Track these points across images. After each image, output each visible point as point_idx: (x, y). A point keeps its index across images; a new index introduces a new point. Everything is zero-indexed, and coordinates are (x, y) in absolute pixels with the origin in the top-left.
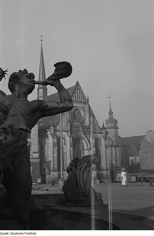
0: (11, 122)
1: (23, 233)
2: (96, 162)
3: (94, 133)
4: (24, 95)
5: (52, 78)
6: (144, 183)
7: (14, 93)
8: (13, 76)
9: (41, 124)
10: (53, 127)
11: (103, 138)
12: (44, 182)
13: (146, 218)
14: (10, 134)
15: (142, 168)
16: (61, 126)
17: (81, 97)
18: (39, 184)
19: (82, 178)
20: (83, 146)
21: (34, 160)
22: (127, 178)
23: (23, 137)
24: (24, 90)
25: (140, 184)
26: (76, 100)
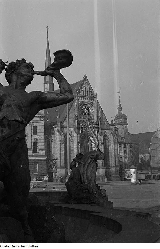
0: (6, 113)
1: (24, 246)
2: (101, 158)
3: (101, 129)
4: (21, 86)
5: (52, 67)
6: (154, 181)
7: (12, 84)
8: (11, 66)
9: (47, 121)
10: (59, 124)
11: (111, 135)
12: (50, 180)
13: (150, 215)
14: (6, 126)
15: (152, 166)
16: (68, 122)
17: (88, 92)
18: (46, 181)
19: (86, 175)
20: (91, 143)
21: (40, 157)
22: (137, 176)
23: (21, 130)
24: (22, 80)
25: (150, 181)
26: (83, 95)
